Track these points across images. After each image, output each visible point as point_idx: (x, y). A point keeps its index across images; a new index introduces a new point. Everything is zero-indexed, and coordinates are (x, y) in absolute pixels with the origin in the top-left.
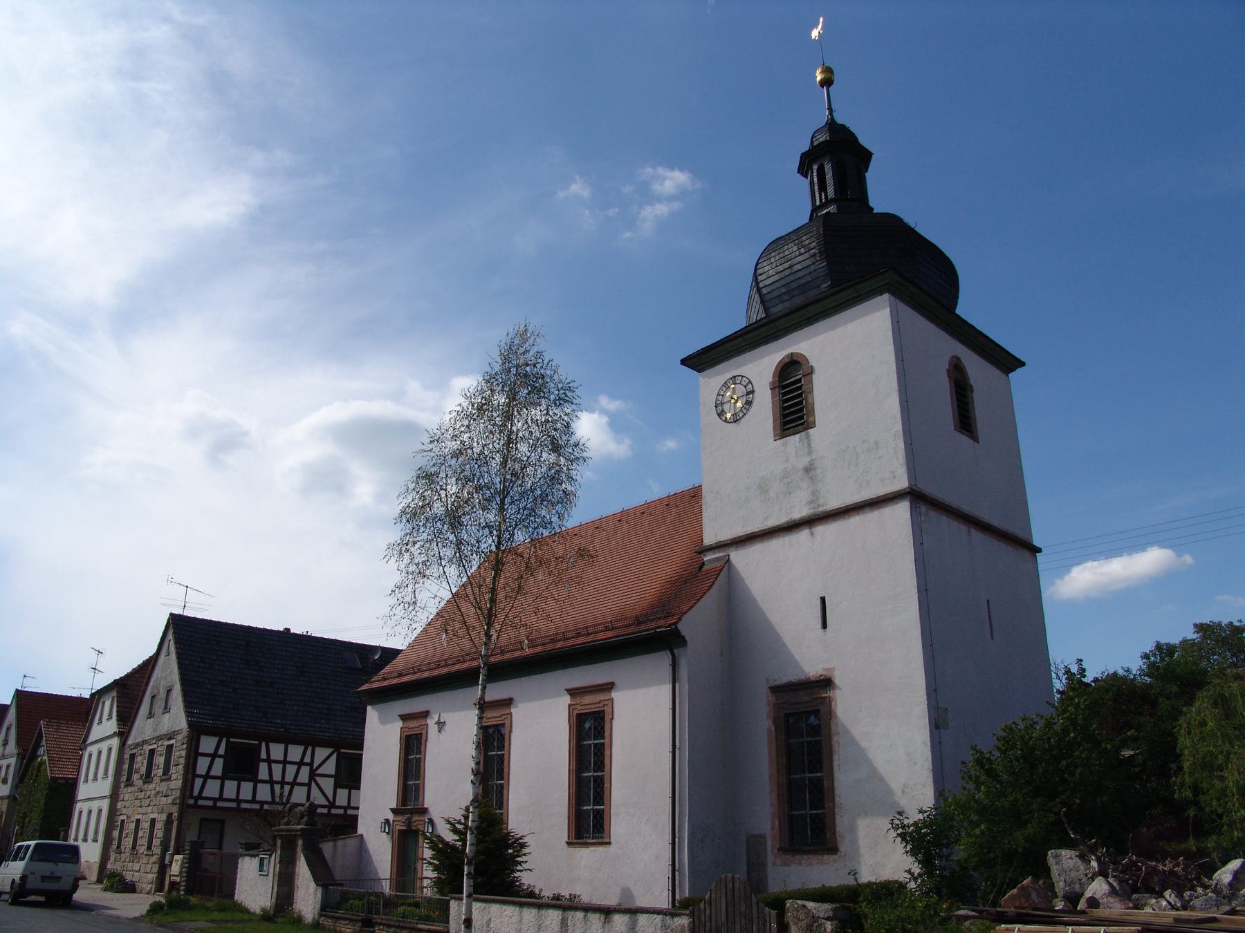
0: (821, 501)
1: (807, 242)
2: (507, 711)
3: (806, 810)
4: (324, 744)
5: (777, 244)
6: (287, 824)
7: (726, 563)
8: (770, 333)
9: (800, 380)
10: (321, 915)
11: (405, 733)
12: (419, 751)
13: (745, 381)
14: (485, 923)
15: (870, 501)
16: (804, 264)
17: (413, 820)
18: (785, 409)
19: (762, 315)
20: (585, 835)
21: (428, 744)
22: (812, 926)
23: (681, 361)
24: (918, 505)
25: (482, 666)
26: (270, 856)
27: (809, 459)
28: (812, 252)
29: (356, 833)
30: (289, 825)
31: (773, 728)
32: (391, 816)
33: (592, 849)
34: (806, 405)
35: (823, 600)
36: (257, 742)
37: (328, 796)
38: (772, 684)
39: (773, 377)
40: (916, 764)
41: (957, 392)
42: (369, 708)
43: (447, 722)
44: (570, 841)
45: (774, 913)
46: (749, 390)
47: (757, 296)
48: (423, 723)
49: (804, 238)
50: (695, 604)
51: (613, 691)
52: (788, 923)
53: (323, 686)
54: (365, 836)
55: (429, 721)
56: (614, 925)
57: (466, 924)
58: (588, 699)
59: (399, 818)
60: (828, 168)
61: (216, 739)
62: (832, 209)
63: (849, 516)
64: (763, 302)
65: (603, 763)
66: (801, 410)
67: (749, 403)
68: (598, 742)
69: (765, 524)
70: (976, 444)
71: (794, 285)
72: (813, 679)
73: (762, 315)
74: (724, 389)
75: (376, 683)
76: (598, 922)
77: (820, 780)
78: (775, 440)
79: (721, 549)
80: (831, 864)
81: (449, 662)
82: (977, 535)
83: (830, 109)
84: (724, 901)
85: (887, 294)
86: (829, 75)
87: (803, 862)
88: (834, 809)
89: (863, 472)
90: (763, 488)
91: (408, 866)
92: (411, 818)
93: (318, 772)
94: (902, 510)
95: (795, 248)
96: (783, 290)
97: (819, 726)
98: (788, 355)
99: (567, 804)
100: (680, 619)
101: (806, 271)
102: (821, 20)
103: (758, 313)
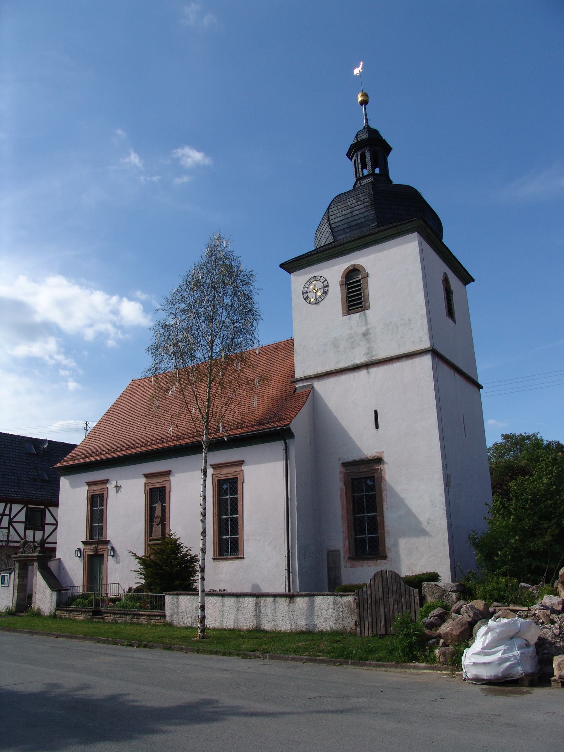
0: (374, 353)
1: (363, 198)
2: (167, 479)
3: (365, 534)
4: (18, 502)
5: (340, 198)
8: (340, 251)
9: (359, 281)
10: (57, 610)
11: (90, 494)
13: (322, 280)
14: (194, 608)
15: (407, 354)
17: (98, 548)
18: (349, 297)
19: (331, 239)
20: (225, 554)
21: (108, 500)
22: (442, 596)
23: (280, 265)
24: (435, 358)
25: (204, 448)
26: (10, 574)
27: (367, 328)
30: (24, 553)
31: (344, 487)
32: (82, 547)
35: (376, 412)
36: (43, 507)
37: (45, 535)
38: (342, 461)
40: (436, 506)
42: (62, 478)
43: (122, 486)
44: (215, 557)
45: (416, 590)
46: (325, 285)
47: (328, 228)
48: (105, 487)
49: (360, 196)
51: (243, 465)
52: (425, 595)
53: (14, 465)
54: (62, 560)
55: (108, 486)
56: (297, 604)
57: (202, 609)
58: (225, 471)
59: (89, 547)
60: (368, 155)
63: (393, 363)
64: (332, 232)
66: (361, 299)
67: (325, 293)
68: (233, 496)
71: (353, 223)
72: (370, 458)
73: (331, 239)
74: (309, 283)
76: (284, 603)
77: (374, 518)
79: (308, 380)
80: (383, 565)
81: (136, 445)
82: (458, 377)
83: (366, 119)
84: (380, 585)
85: (417, 233)
86: (366, 98)
87: (364, 565)
88: (384, 534)
90: (335, 344)
91: (95, 577)
92: (97, 547)
93: (14, 520)
94: (427, 360)
95: (354, 201)
96: (346, 226)
97: (374, 486)
100: (291, 422)
101: (362, 216)
102: (361, 63)
103: (326, 238)
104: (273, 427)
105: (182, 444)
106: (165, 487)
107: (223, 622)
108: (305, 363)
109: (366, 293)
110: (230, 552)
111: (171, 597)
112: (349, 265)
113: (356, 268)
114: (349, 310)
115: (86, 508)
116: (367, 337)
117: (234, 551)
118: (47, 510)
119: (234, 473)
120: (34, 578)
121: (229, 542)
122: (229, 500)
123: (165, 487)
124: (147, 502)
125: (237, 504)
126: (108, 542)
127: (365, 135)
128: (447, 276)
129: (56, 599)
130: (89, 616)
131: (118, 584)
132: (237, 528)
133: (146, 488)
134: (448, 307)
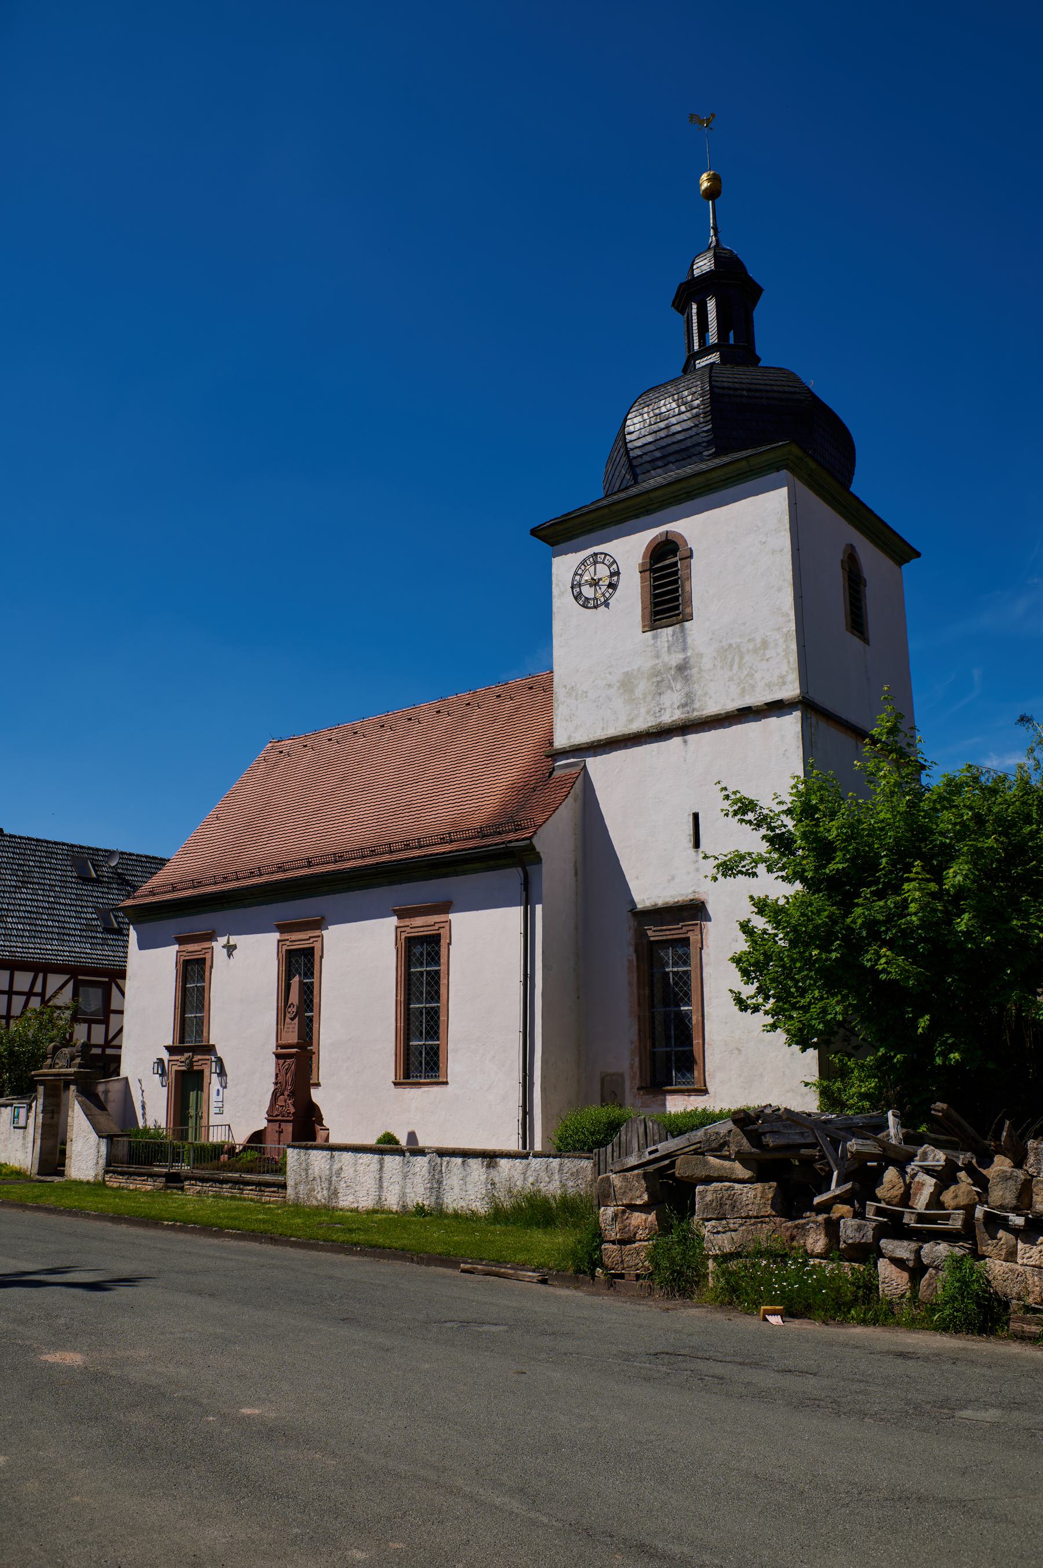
1: (689, 398)
2: (317, 933)
6: (51, 1067)
7: (581, 770)
9: (675, 564)
10: (107, 1172)
11: (182, 958)
12: (202, 978)
16: (685, 425)
18: (656, 596)
23: (531, 530)
28: (694, 411)
29: (119, 1075)
32: (165, 1056)
33: (425, 1089)
34: (683, 593)
35: (696, 817)
36: (107, 980)
39: (643, 557)
41: (850, 587)
44: (398, 1080)
47: (624, 459)
50: (551, 815)
58: (419, 921)
60: (711, 305)
61: (31, 975)
62: (714, 358)
65: (438, 993)
66: (676, 599)
67: (612, 586)
69: (629, 727)
70: (867, 645)
75: (142, 897)
78: (643, 632)
89: (748, 675)
90: (627, 684)
92: (193, 1058)
95: (674, 405)
96: (658, 454)
98: (663, 532)
99: (394, 1039)
100: (535, 833)
104: (503, 843)
105: (344, 869)
106: (313, 948)
107: (380, 1199)
108: (571, 721)
109: (686, 587)
110: (423, 1071)
111: (296, 1151)
112: (658, 533)
113: (669, 538)
114: (655, 621)
115: (175, 983)
116: (686, 674)
117: (432, 1069)
118: (113, 985)
119: (434, 925)
120: (70, 1112)
121: (424, 1053)
122: (425, 975)
123: (313, 948)
124: (280, 976)
125: (438, 983)
126: (210, 1049)
127: (709, 264)
128: (856, 551)
129: (105, 1153)
130: (160, 1182)
131: (227, 1127)
132: (438, 1028)
133: (280, 950)
134: (852, 612)
